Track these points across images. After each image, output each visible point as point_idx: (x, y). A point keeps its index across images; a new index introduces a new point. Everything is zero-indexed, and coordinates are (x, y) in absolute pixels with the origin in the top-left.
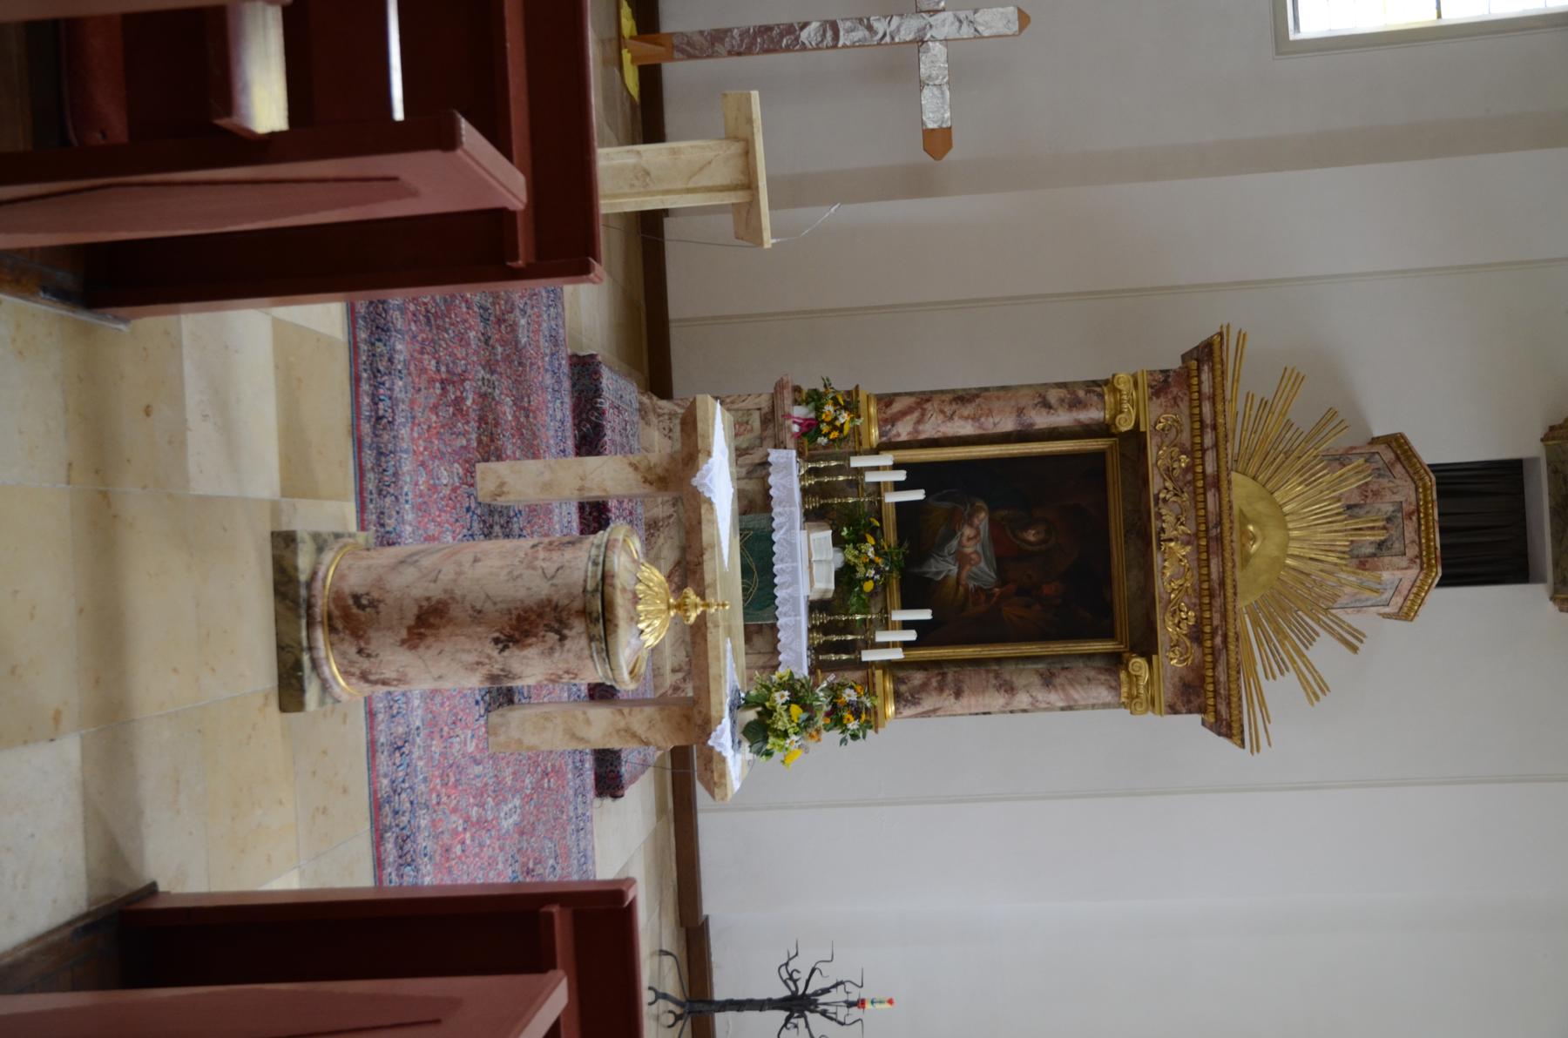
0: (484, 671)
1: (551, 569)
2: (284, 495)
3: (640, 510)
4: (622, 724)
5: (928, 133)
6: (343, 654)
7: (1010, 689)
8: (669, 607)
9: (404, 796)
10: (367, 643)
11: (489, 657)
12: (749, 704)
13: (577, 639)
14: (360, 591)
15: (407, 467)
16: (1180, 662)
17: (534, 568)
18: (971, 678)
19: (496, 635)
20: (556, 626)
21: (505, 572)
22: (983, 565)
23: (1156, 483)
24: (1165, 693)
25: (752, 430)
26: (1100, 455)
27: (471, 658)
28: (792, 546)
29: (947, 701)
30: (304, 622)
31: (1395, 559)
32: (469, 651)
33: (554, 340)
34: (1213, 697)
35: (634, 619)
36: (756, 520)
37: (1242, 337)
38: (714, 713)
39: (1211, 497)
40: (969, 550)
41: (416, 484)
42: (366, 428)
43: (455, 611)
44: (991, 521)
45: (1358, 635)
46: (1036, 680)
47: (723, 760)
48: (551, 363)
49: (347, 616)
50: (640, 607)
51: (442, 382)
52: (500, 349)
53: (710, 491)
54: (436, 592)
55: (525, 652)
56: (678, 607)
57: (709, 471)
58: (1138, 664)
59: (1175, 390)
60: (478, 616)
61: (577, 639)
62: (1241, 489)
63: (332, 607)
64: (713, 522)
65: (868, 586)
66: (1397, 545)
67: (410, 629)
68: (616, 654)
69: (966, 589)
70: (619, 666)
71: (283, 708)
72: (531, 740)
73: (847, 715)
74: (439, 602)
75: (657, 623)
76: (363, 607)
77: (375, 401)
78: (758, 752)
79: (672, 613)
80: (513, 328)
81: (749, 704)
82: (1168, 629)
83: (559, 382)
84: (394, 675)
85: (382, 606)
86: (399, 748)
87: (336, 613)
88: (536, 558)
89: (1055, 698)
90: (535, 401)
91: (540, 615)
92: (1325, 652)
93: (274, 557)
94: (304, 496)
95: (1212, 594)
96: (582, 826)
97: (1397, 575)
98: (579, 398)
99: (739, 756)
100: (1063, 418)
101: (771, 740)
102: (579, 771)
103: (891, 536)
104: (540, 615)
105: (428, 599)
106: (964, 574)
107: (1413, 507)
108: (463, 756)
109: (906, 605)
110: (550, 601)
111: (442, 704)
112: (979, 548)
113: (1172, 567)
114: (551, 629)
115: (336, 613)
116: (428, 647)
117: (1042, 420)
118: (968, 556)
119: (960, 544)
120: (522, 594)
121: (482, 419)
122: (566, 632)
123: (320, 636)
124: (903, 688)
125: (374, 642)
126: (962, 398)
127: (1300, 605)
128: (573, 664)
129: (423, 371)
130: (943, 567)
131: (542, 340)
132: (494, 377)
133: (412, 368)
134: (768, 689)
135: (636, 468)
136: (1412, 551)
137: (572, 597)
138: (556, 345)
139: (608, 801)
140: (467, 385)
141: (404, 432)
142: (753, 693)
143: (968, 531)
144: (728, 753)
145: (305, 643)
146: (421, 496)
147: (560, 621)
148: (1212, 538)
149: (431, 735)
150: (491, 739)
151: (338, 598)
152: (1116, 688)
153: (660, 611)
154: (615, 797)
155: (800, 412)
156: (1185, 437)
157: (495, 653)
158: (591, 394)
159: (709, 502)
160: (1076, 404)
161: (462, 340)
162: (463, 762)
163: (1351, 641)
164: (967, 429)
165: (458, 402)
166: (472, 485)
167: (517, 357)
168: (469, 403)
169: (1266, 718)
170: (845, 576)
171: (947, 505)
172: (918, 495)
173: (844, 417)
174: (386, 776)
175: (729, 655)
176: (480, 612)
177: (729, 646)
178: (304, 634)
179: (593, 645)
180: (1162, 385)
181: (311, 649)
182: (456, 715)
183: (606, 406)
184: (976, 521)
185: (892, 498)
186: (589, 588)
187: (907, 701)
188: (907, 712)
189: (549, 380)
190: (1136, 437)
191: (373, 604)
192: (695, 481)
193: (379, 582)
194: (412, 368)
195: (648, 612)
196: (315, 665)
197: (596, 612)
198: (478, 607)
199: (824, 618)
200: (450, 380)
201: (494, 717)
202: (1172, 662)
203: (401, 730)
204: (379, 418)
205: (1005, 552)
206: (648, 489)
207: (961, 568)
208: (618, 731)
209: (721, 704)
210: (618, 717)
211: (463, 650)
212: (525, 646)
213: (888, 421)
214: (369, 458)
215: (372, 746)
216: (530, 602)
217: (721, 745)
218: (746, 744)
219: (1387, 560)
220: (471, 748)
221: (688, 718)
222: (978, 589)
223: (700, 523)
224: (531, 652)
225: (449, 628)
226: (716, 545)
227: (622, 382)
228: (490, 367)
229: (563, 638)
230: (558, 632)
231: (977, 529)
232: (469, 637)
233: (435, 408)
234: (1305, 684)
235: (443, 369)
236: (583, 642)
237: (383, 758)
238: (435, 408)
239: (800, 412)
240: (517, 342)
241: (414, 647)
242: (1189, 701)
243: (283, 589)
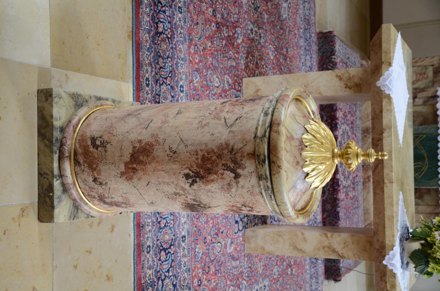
0: (181, 200)
1: (231, 118)
2: (55, 64)
3: (358, 122)
4: (326, 243)
6: (85, 181)
8: (334, 156)
9: (167, 281)
10: (99, 174)
11: (183, 189)
12: (414, 237)
13: (249, 180)
14: (97, 135)
15: (183, 69)
17: (219, 119)
19: (187, 171)
20: (232, 165)
21: (197, 121)
25: (427, 78)
27: (171, 189)
30: (56, 157)
32: (168, 184)
33: (307, 21)
35: (300, 163)
36: (427, 129)
38: (387, 242)
41: (191, 81)
42: (145, 37)
43: (158, 152)
47: (394, 276)
48: (304, 33)
49: (86, 153)
50: (304, 153)
51: (217, 23)
52: (266, 16)
53: (390, 89)
54: (146, 136)
55: (209, 187)
56: (341, 156)
57: (389, 76)
61: (249, 180)
63: (78, 146)
64: (391, 111)
67: (126, 164)
68: (280, 192)
70: (284, 203)
71: (40, 219)
72: (270, 248)
74: (147, 144)
75: (322, 167)
76: (96, 147)
77: (155, 21)
78: (421, 272)
79: (336, 161)
81: (414, 237)
83: (310, 45)
84: (120, 200)
85: (109, 146)
86: (165, 250)
87: (80, 151)
88: (222, 111)
91: (220, 156)
93: (38, 107)
94: (78, 70)
98: (322, 57)
99: (407, 273)
101: (432, 265)
104: (220, 156)
105: (140, 141)
108: (223, 255)
110: (227, 145)
111: (207, 222)
114: (228, 168)
115: (80, 151)
116: (139, 179)
120: (207, 138)
122: (239, 171)
123: (68, 167)
125: (103, 173)
128: (248, 199)
129: (200, 12)
131: (298, 20)
132: (261, 31)
133: (191, 8)
134: (430, 228)
135: (341, 79)
137: (245, 142)
138: (308, 24)
139: (332, 282)
140: (239, 30)
141: (183, 47)
142: (419, 230)
144: (398, 270)
145: (56, 172)
146: (195, 90)
147: (235, 162)
149: (196, 241)
150: (246, 245)
151: (82, 140)
153: (325, 158)
154: (336, 280)
157: (187, 186)
158: (329, 54)
159: (389, 97)
162: (222, 259)
165: (230, 40)
166: (240, 91)
167: (278, 24)
168: (239, 41)
174: (150, 268)
175: (401, 203)
176: (175, 152)
177: (401, 197)
178: (56, 165)
179: (261, 183)
181: (61, 176)
182: (219, 229)
183: (338, 60)
186: (259, 134)
189: (302, 42)
191: (104, 145)
192: (378, 84)
193: (110, 130)
194: (191, 8)
195: (312, 158)
196: (65, 189)
197: (258, 156)
198: (174, 149)
201: (249, 232)
203: (167, 237)
204: (158, 34)
206: (348, 93)
208: (324, 247)
209: (393, 236)
210: (324, 238)
211: (164, 183)
212: (209, 182)
214: (146, 57)
215: (139, 248)
216: (213, 146)
217: (392, 265)
218: (412, 266)
220: (230, 250)
221: (371, 244)
223: (381, 112)
224: (214, 187)
225: (153, 164)
226: (392, 126)
227: (349, 51)
228: (258, 24)
229: (237, 176)
230: (233, 171)
232: (167, 172)
233: (210, 38)
235: (219, 16)
236: (254, 180)
237: (149, 258)
238: (210, 38)
240: (280, 16)
241: (129, 179)
243: (43, 131)
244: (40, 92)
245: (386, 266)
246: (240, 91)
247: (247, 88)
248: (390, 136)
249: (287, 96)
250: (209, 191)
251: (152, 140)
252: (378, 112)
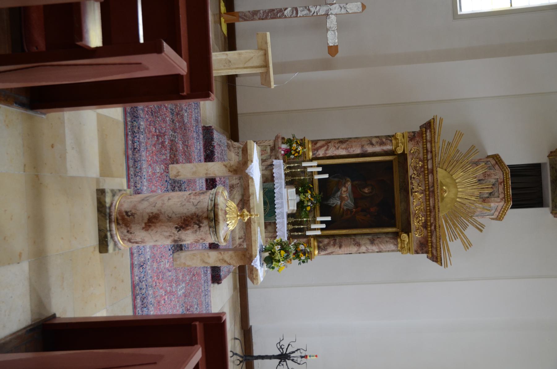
0: (172, 238)
2: (101, 176)
3: (227, 181)
4: (221, 257)
6: (122, 233)
7: (359, 245)
8: (238, 216)
9: (143, 283)
10: (130, 229)
11: (174, 234)
12: (266, 250)
13: (205, 227)
14: (128, 210)
15: (144, 166)
16: (419, 235)
17: (190, 202)
19: (176, 226)
20: (198, 222)
21: (179, 203)
22: (349, 201)
23: (411, 172)
24: (414, 246)
25: (267, 153)
26: (391, 162)
27: (167, 234)
28: (281, 194)
29: (336, 249)
30: (108, 221)
31: (496, 199)
32: (167, 232)
33: (197, 121)
34: (431, 248)
35: (225, 220)
36: (269, 185)
37: (441, 120)
38: (254, 254)
39: (430, 177)
40: (344, 196)
41: (148, 172)
42: (130, 152)
43: (162, 217)
44: (352, 185)
45: (483, 226)
46: (368, 242)
47: (257, 270)
48: (196, 129)
49: (123, 219)
50: (227, 216)
51: (157, 136)
52: (177, 124)
53: (252, 174)
54: (155, 210)
56: (241, 216)
57: (252, 167)
58: (404, 236)
59: (417, 139)
60: (170, 219)
61: (205, 227)
62: (441, 174)
63: (118, 216)
64: (253, 186)
65: (308, 208)
66: (496, 194)
67: (145, 224)
68: (219, 232)
69: (343, 209)
70: (220, 237)
71: (101, 252)
72: (189, 263)
73: (301, 254)
74: (156, 214)
75: (233, 221)
76: (129, 216)
77: (133, 142)
78: (269, 267)
79: (239, 218)
80: (182, 116)
81: (266, 250)
82: (415, 224)
83: (199, 136)
84: (140, 240)
85: (135, 215)
86: (142, 266)
87: (119, 218)
88: (190, 198)
89: (375, 248)
90: (190, 142)
91: (192, 219)
92: (471, 232)
93: (97, 198)
94: (108, 176)
95: (431, 211)
96: (207, 294)
97: (496, 204)
98: (206, 142)
99: (262, 269)
100: (378, 149)
101: (274, 263)
102: (206, 274)
103: (317, 191)
104: (192, 219)
105: (152, 213)
106: (342, 204)
107: (502, 180)
108: (165, 269)
109: (322, 215)
110: (195, 214)
111: (157, 250)
112: (348, 195)
113: (416, 202)
114: (196, 224)
115: (119, 218)
116: (152, 230)
117: (370, 149)
118: (344, 198)
119: (341, 193)
120: (185, 211)
121: (171, 149)
122: (201, 225)
123: (114, 226)
124: (321, 245)
126: (342, 141)
127: (462, 215)
129: (150, 132)
130: (335, 202)
131: (193, 121)
132: (176, 134)
134: (273, 245)
135: (226, 166)
136: (502, 196)
137: (203, 212)
138: (197, 123)
139: (216, 285)
140: (166, 137)
141: (144, 153)
142: (268, 246)
143: (344, 189)
144: (259, 268)
145: (108, 229)
146: (150, 176)
147: (199, 221)
148: (431, 191)
149: (153, 261)
150: (174, 263)
151: (120, 212)
152: (397, 245)
153: (235, 217)
154: (218, 283)
155: (284, 146)
156: (421, 155)
157: (176, 232)
159: (252, 178)
160: (382, 144)
161: (164, 121)
162: (164, 271)
163: (480, 228)
164: (343, 152)
165: (163, 143)
166: (168, 173)
167: (183, 127)
168: (167, 143)
169: (450, 255)
170: (300, 205)
171: (336, 179)
172: (326, 176)
173: (300, 148)
174: (137, 276)
175: (259, 233)
176: (170, 218)
177: (259, 230)
178: (108, 225)
179: (211, 229)
180: (413, 137)
181: (110, 231)
182: (162, 254)
183: (215, 144)
184: (347, 185)
185: (317, 177)
186: (209, 209)
187: (322, 249)
188: (322, 253)
189: (195, 135)
190: (404, 155)
191: (133, 215)
192: (247, 171)
193: (135, 207)
195: (230, 218)
196: (112, 236)
197: (212, 218)
199: (293, 220)
201: (176, 255)
202: (416, 235)
203: (142, 259)
205: (357, 197)
206: (230, 174)
207: (341, 202)
208: (220, 260)
209: (256, 250)
210: (220, 255)
213: (315, 150)
214: (131, 163)
216: (188, 214)
217: (256, 265)
218: (265, 265)
219: (493, 199)
220: (167, 266)
221: (245, 255)
222: (348, 210)
223: (249, 186)
224: (189, 232)
226: (254, 194)
227: (221, 136)
228: (174, 130)
229: (200, 227)
230: (198, 225)
231: (347, 188)
232: (167, 226)
233: (154, 145)
234: (464, 243)
235: (157, 131)
236: (207, 228)
237: (136, 270)
238: (154, 145)
239: (284, 146)
240: (184, 122)
241: (147, 230)
242: (422, 249)
243: (100, 209)
244: (98, 190)
245: (253, 266)
246: (168, 173)
247: (172, 170)
248: (253, 198)
249: (219, 192)
250: (187, 234)
251: (158, 212)
252: (247, 186)
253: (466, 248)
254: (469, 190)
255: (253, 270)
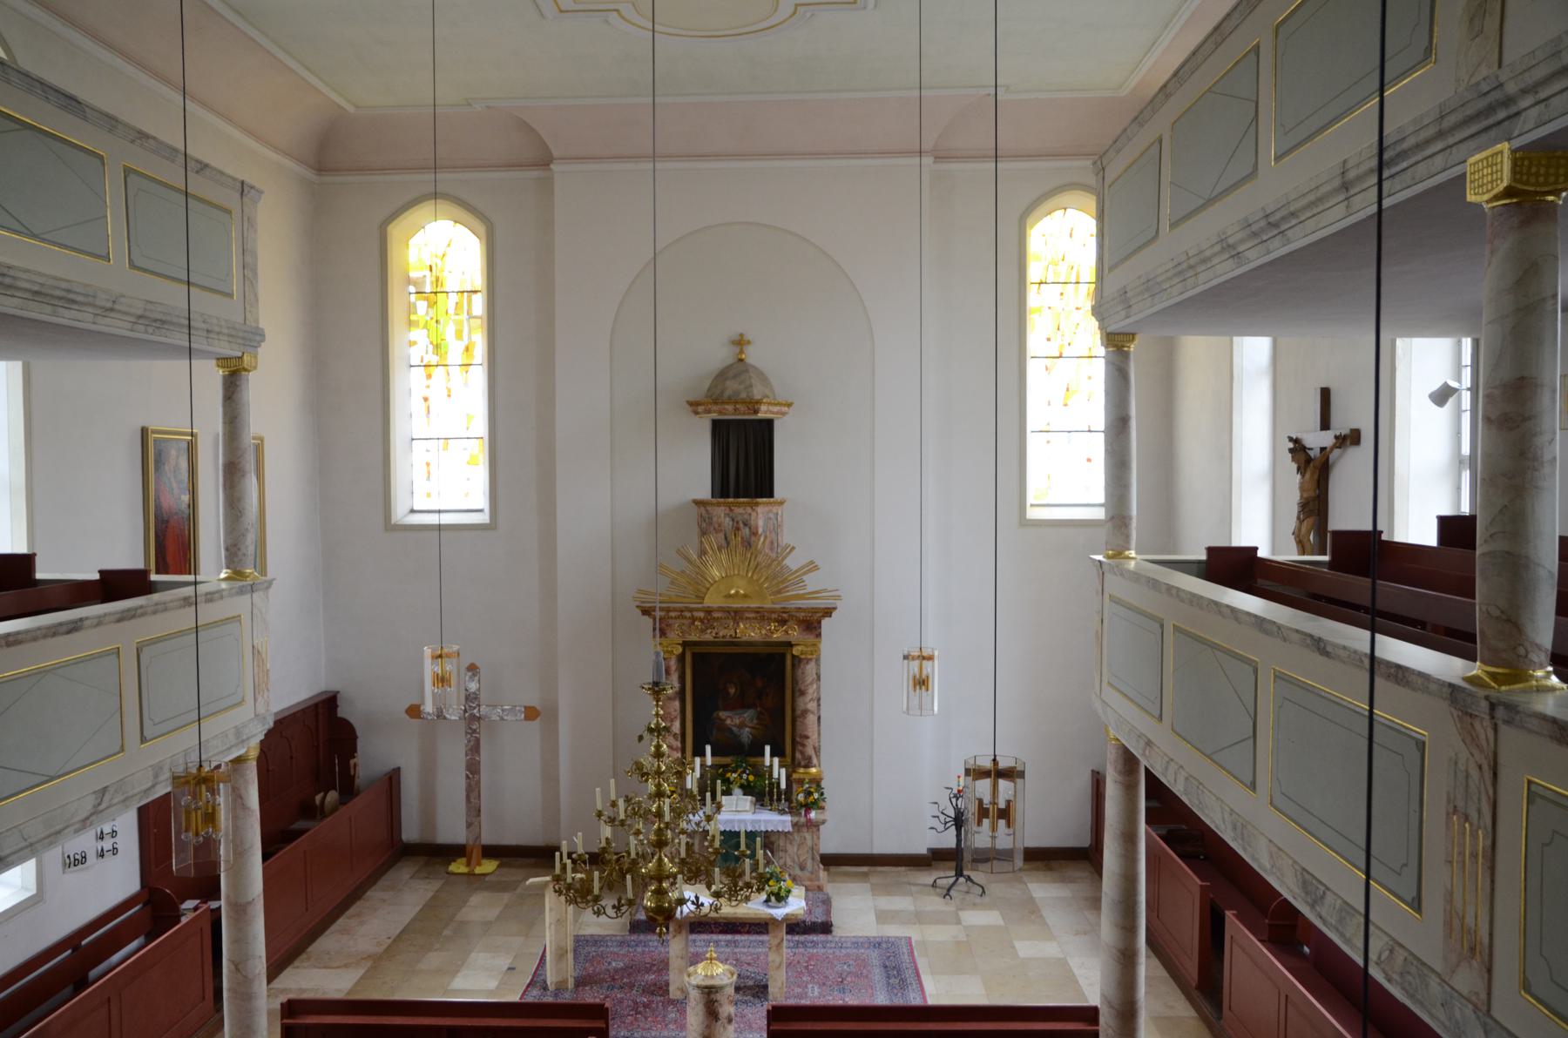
5: (527, 718)
7: (805, 712)
13: (718, 997)
18: (798, 732)
23: (708, 637)
24: (810, 639)
26: (694, 655)
28: (727, 821)
29: (810, 743)
33: (622, 944)
34: (812, 622)
37: (640, 591)
39: (716, 615)
44: (725, 709)
60: (708, 1027)
61: (718, 997)
62: (713, 600)
65: (751, 778)
73: (811, 799)
80: (616, 970)
82: (777, 636)
89: (811, 690)
90: (648, 960)
92: (792, 562)
95: (762, 616)
96: (840, 945)
102: (815, 944)
103: (727, 760)
109: (763, 755)
113: (751, 633)
118: (739, 722)
127: (780, 579)
130: (746, 735)
136: (749, 510)
143: (728, 722)
148: (737, 615)
156: (687, 622)
161: (621, 1001)
165: (646, 1006)
167: (630, 970)
169: (825, 590)
170: (747, 789)
172: (708, 748)
185: (709, 760)
188: (815, 761)
190: (685, 644)
199: (767, 798)
200: (636, 1008)
202: (795, 634)
205: (740, 704)
228: (632, 986)
229: (759, 402)
234: (810, 571)
253: (816, 568)
254: (737, 560)
255: (786, 918)
